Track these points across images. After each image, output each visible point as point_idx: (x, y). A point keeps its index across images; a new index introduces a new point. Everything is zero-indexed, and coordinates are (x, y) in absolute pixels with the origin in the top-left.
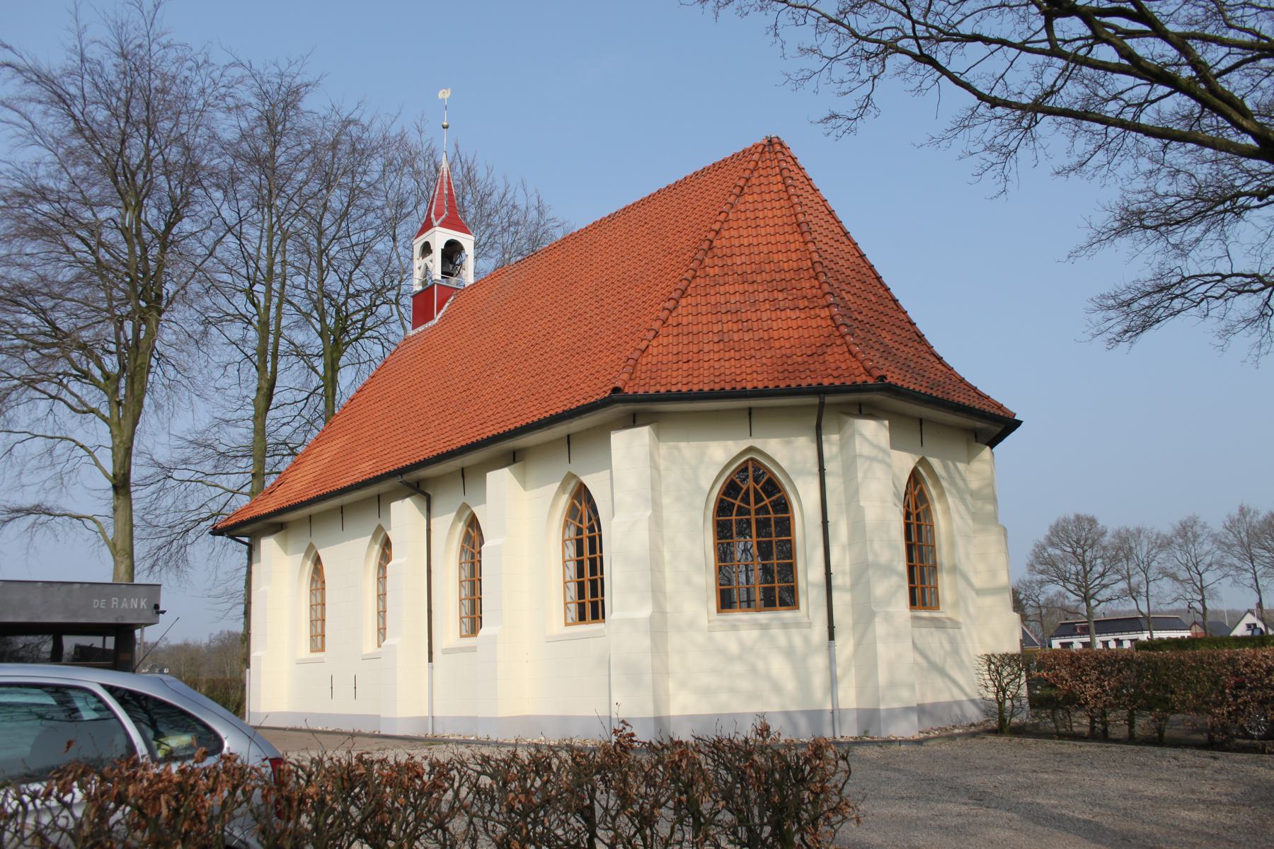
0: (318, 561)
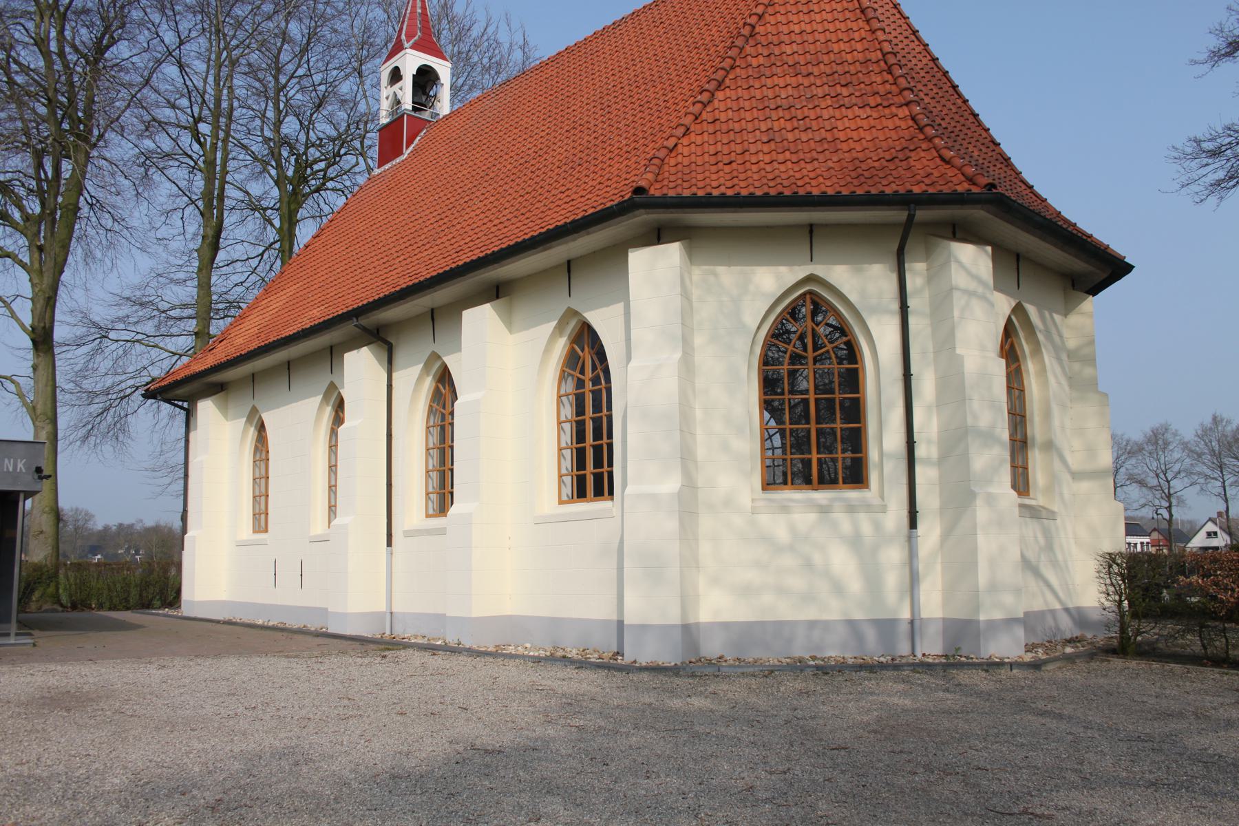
0: (261, 427)
